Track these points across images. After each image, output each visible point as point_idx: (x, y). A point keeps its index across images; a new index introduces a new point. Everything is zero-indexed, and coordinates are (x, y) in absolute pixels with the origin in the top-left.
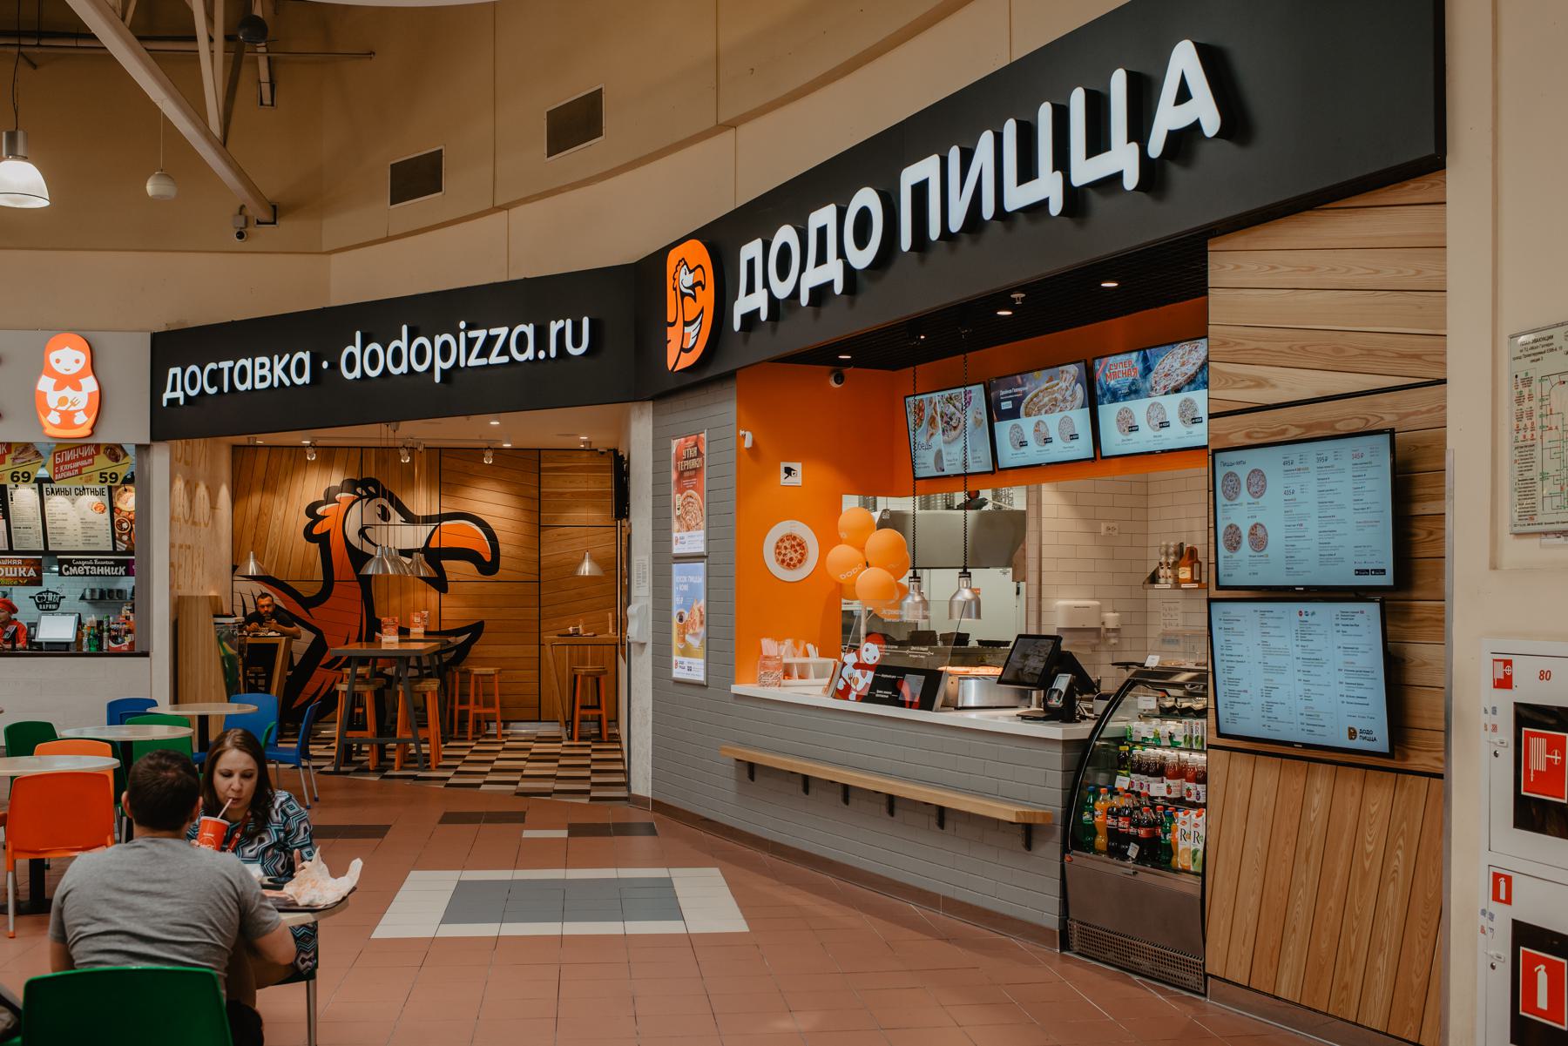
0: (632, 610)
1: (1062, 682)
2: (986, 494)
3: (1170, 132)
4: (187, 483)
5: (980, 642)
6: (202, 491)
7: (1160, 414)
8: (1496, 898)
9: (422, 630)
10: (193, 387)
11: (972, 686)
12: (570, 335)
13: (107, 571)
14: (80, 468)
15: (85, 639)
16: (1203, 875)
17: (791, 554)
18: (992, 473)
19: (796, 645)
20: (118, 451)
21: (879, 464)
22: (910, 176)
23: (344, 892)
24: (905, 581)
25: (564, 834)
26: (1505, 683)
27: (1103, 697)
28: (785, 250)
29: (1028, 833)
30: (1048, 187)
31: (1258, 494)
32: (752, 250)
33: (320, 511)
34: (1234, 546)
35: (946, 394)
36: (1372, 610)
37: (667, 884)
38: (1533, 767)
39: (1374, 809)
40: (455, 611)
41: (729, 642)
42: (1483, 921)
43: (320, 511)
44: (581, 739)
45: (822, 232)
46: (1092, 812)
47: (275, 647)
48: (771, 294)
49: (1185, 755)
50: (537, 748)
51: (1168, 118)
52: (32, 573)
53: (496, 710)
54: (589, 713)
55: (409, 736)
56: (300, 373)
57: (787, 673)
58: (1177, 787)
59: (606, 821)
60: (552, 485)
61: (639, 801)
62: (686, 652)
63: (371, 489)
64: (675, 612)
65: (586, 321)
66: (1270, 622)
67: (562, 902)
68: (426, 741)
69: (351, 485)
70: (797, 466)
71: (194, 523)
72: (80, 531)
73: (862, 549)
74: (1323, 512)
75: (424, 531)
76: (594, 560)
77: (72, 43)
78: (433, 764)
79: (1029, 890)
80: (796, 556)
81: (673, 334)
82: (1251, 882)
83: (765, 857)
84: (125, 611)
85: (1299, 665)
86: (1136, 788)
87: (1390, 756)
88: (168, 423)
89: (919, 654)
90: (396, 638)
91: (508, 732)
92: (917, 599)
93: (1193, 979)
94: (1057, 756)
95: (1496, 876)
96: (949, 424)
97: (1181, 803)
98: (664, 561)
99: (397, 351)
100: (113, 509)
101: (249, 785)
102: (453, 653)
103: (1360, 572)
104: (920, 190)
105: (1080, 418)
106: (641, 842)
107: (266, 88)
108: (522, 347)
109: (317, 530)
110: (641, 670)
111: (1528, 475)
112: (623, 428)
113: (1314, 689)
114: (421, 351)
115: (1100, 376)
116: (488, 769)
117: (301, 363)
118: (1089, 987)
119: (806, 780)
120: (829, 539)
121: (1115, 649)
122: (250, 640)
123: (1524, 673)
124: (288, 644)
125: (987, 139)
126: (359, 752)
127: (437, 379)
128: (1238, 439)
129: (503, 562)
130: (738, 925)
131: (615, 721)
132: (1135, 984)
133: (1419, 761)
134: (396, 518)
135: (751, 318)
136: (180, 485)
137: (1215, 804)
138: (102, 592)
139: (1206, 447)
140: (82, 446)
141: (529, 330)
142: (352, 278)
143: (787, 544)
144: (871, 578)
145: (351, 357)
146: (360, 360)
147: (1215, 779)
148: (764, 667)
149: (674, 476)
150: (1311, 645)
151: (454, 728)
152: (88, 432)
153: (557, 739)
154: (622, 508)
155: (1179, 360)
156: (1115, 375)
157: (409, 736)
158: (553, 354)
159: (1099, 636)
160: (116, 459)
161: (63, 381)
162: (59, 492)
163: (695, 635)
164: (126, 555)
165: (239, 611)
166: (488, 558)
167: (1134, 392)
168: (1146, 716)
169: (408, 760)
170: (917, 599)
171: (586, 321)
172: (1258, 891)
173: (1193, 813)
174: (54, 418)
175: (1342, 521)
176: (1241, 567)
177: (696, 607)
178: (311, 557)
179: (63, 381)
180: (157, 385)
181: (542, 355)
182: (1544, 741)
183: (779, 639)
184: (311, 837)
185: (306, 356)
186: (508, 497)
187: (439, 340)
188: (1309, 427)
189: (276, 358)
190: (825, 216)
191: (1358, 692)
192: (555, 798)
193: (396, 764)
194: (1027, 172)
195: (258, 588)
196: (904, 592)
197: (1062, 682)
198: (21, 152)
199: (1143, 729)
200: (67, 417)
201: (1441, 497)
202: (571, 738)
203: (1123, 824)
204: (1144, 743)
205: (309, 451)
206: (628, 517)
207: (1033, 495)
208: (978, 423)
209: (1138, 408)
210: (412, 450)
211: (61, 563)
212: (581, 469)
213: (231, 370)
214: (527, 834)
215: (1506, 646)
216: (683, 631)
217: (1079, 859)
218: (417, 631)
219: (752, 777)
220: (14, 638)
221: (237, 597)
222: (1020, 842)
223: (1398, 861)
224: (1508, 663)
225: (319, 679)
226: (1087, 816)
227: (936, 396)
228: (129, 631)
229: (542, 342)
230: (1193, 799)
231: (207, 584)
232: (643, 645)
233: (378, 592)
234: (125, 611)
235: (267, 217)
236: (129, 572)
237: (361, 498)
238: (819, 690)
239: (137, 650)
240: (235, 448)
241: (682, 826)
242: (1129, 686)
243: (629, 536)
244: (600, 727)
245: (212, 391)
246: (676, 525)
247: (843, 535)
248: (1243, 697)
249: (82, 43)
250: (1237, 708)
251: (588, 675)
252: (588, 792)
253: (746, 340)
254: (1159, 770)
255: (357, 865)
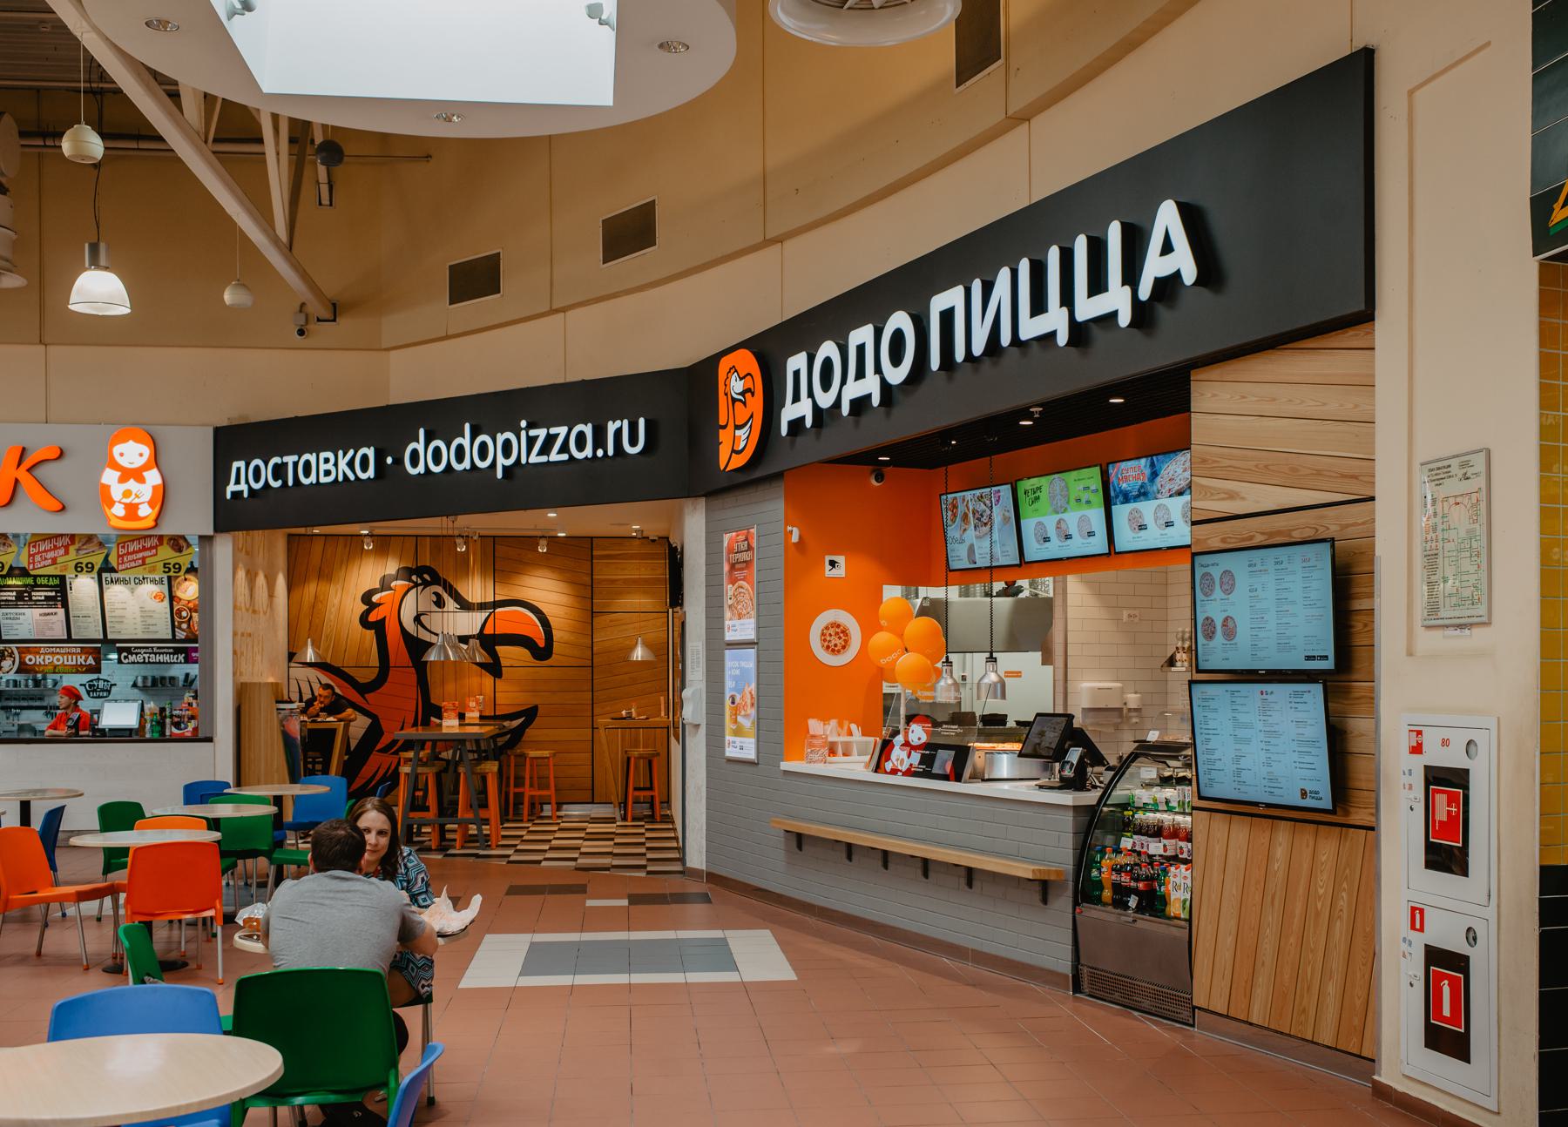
0: (686, 693)
1: (1074, 755)
2: (1023, 583)
3: (1157, 280)
4: (248, 572)
5: (1018, 723)
6: (261, 580)
7: (1160, 520)
8: (1413, 927)
9: (477, 714)
10: (257, 479)
11: (1004, 761)
12: (626, 435)
13: (166, 658)
14: (144, 559)
15: (148, 726)
16: (1190, 920)
17: (835, 640)
18: (1019, 566)
19: (841, 725)
20: (182, 542)
21: (919, 557)
22: (939, 303)
23: (467, 922)
24: (939, 665)
25: (625, 902)
26: (1417, 749)
27: (1109, 769)
28: (827, 363)
29: (1045, 888)
30: (1055, 320)
31: (1228, 592)
32: (797, 362)
33: (375, 598)
34: (1210, 636)
35: (978, 492)
36: (1317, 689)
37: (724, 943)
38: (1438, 818)
39: (1324, 859)
40: (510, 696)
41: (782, 719)
42: (1404, 947)
43: (375, 598)
44: (634, 819)
45: (861, 349)
46: (1099, 870)
47: (334, 731)
48: (815, 405)
49: (1179, 818)
50: (592, 828)
51: (1155, 266)
52: (91, 661)
53: (551, 792)
54: (641, 794)
55: (470, 816)
56: (364, 468)
57: (833, 752)
58: (1171, 844)
59: (662, 889)
60: (604, 572)
61: (695, 873)
62: (738, 732)
63: (427, 577)
64: (728, 695)
65: (642, 422)
66: (1239, 700)
67: (629, 958)
68: (486, 821)
69: (406, 573)
70: (841, 559)
71: (254, 612)
72: (139, 620)
73: (901, 636)
74: (1279, 609)
75: (479, 617)
76: (646, 645)
77: (133, 145)
78: (493, 842)
79: (1045, 940)
80: (840, 642)
81: (724, 436)
82: (1229, 924)
83: (811, 920)
84: (188, 697)
85: (1262, 736)
86: (1137, 848)
87: (1333, 812)
88: (231, 515)
89: (951, 732)
90: (456, 722)
91: (562, 813)
92: (950, 681)
93: (1185, 1014)
94: (1068, 819)
95: (1413, 909)
96: (984, 521)
97: (1175, 859)
98: (717, 646)
99: (460, 449)
100: (172, 598)
101: (384, 841)
102: (508, 736)
103: (1309, 658)
104: (947, 316)
105: (1096, 516)
106: (697, 910)
107: (325, 189)
108: (581, 444)
109: (372, 618)
110: (697, 746)
111: (1433, 578)
112: (677, 520)
113: (1274, 757)
114: (483, 450)
115: (1113, 479)
116: (546, 847)
117: (365, 458)
118: (1096, 1020)
119: (849, 848)
120: (870, 626)
121: (1135, 727)
122: (310, 726)
123: (1430, 740)
124: (346, 728)
125: (1004, 275)
126: (419, 833)
127: (499, 475)
128: (1216, 544)
129: (556, 647)
130: (787, 973)
131: (667, 802)
132: (1136, 1019)
133: (1359, 817)
134: (451, 604)
135: (796, 425)
136: (241, 574)
137: (1198, 860)
138: (154, 679)
139: (1189, 546)
140: (145, 537)
141: (588, 429)
142: (411, 376)
143: (831, 631)
144: (908, 661)
145: (415, 453)
146: (424, 456)
147: (1198, 837)
148: (811, 745)
149: (726, 568)
150: (1271, 720)
151: (511, 810)
152: (152, 524)
153: (612, 820)
154: (676, 596)
155: (1176, 468)
156: (1126, 479)
157: (470, 816)
158: (611, 452)
159: (1121, 716)
160: (180, 550)
161: (127, 474)
162: (117, 581)
163: (747, 716)
164: (188, 641)
165: (295, 697)
166: (542, 644)
167: (1143, 494)
168: (1148, 785)
169: (469, 840)
170: (950, 681)
171: (642, 422)
172: (1234, 931)
173: (1183, 867)
174: (118, 510)
175: (1294, 615)
176: (1217, 654)
177: (747, 690)
178: (367, 644)
179: (127, 474)
180: (221, 477)
181: (600, 453)
182: (1445, 796)
183: (825, 719)
184: (428, 885)
185: (370, 452)
186: (561, 584)
187: (501, 438)
188: (1271, 535)
189: (340, 453)
190: (862, 335)
191: (1308, 759)
192: (614, 872)
193: (458, 844)
194: (1039, 307)
195: (313, 673)
196: (939, 673)
197: (1074, 755)
198: (103, 262)
199: (1144, 796)
200: (132, 510)
201: (1371, 595)
202: (624, 818)
203: (1125, 879)
204: (1145, 808)
205: (367, 540)
206: (681, 605)
207: (1060, 585)
208: (1006, 520)
209: (1146, 508)
210: (467, 539)
211: (120, 651)
212: (632, 557)
213: (296, 464)
214: (590, 903)
215: (1420, 719)
216: (735, 712)
217: (1091, 912)
218: (473, 715)
219: (800, 847)
220: (77, 726)
221: (293, 684)
222: (1037, 897)
223: (1343, 902)
224: (1419, 733)
225: (376, 763)
226: (1095, 873)
227: (968, 495)
228: (192, 718)
229: (599, 441)
230: (1185, 856)
231: (266, 672)
232: (697, 726)
233: (433, 677)
234: (188, 697)
235: (327, 315)
236: (188, 660)
237: (416, 585)
238: (861, 767)
239: (201, 735)
240: (290, 535)
241: (733, 894)
242: (1134, 757)
243: (683, 624)
244: (652, 807)
245: (276, 484)
246: (728, 614)
247: (883, 623)
248: (1218, 765)
249: (143, 145)
250: (1214, 774)
251: (641, 757)
252: (644, 867)
253: (793, 444)
254: (1157, 832)
255: (477, 900)
